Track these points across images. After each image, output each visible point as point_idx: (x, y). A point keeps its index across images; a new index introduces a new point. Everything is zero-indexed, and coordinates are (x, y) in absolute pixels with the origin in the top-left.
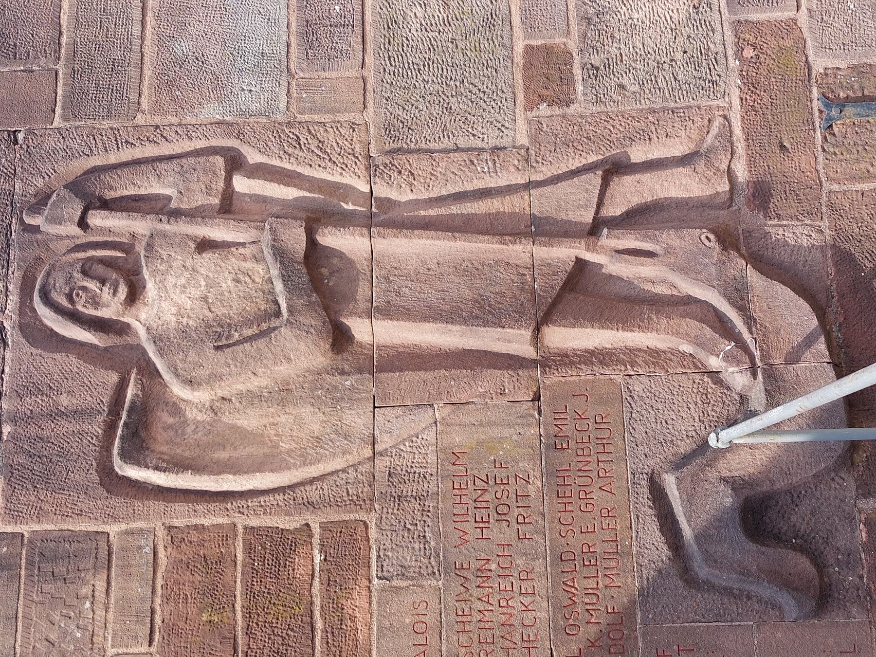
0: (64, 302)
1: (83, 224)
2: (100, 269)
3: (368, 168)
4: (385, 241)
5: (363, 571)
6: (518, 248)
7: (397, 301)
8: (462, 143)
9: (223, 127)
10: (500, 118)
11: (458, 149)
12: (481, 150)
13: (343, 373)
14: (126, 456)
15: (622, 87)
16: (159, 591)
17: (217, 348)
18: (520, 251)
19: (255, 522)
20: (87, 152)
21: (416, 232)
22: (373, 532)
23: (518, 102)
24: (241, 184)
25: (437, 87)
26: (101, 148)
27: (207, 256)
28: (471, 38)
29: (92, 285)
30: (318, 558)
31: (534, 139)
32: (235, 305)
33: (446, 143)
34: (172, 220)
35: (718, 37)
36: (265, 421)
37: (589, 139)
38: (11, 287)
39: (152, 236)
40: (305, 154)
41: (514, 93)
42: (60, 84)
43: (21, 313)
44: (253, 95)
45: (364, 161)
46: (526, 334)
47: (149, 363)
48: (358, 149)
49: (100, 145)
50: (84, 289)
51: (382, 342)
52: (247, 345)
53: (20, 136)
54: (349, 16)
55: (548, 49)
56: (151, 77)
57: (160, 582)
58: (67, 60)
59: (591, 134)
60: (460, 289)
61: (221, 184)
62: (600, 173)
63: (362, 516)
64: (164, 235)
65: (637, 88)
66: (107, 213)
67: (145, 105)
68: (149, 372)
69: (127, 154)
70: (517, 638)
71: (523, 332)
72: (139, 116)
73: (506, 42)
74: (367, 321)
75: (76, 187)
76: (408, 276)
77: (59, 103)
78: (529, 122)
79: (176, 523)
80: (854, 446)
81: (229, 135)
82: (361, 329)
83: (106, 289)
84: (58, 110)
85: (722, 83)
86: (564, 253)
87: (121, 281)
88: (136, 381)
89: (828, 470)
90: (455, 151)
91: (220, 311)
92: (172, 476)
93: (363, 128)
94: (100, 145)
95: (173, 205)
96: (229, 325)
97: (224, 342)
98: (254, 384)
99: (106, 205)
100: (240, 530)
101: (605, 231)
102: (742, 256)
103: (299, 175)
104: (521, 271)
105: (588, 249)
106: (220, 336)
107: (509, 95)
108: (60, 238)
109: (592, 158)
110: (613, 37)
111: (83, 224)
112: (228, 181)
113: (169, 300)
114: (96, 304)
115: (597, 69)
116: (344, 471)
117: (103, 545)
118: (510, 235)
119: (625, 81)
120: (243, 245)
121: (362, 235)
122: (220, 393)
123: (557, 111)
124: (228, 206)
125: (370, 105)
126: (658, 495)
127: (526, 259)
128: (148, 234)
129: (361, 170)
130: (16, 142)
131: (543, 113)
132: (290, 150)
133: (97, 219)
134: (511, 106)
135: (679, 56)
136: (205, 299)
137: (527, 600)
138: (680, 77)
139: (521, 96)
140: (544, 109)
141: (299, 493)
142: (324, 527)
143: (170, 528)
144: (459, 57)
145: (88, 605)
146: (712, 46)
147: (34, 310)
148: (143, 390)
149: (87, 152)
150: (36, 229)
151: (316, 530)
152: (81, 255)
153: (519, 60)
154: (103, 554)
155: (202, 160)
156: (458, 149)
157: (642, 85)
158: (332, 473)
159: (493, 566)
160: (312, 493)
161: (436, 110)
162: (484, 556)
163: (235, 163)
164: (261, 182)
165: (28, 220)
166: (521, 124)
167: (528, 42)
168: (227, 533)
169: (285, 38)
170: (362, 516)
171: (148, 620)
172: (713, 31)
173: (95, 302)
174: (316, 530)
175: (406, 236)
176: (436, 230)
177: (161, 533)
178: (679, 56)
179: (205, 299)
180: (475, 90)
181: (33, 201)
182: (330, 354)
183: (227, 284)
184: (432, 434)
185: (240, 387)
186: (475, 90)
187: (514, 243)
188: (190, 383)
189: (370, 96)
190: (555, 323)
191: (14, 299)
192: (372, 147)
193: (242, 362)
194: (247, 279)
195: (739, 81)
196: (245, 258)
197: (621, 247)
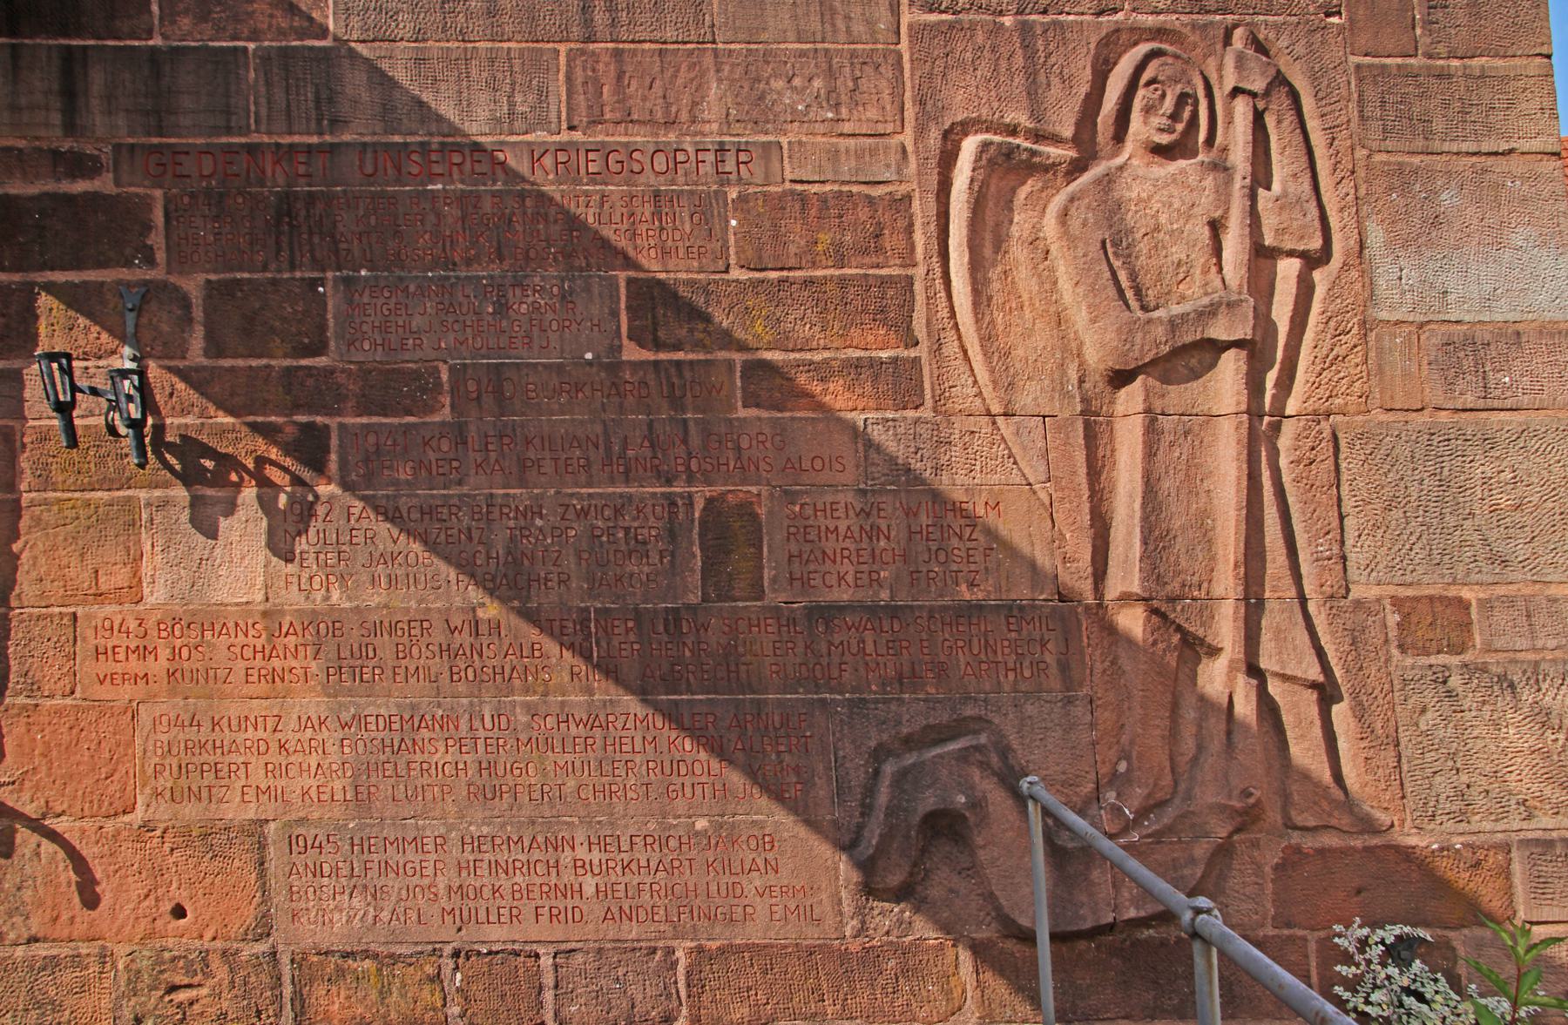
0: (1145, 77)
1: (1236, 92)
2: (1186, 114)
3: (1315, 413)
4: (1232, 431)
5: (872, 404)
6: (1231, 581)
7: (1164, 445)
8: (1349, 523)
9: (1357, 248)
10: (1381, 566)
11: (1341, 518)
12: (1342, 543)
13: (1081, 381)
14: (985, 145)
15: (1424, 711)
16: (845, 188)
17: (1103, 243)
18: (1227, 582)
19: (918, 287)
20: (1320, 95)
21: (1245, 466)
22: (910, 414)
23: (1401, 589)
24: (1288, 269)
25: (1415, 495)
26: (1326, 110)
27: (1206, 231)
28: (1476, 536)
29: (1169, 104)
30: (884, 355)
31: (1358, 603)
32: (1153, 262)
33: (1348, 506)
34: (1247, 191)
35: (1487, 826)
36: (1025, 297)
37: (1361, 669)
38: (1161, 17)
39: (1226, 169)
40: (1328, 343)
41: (1411, 584)
42: (1399, 60)
43: (1132, 29)
44: (1398, 283)
45: (1323, 409)
46: (1135, 587)
47: (1084, 169)
48: (1337, 401)
49: (1329, 109)
50: (1163, 96)
51: (1117, 426)
52: (1108, 275)
53: (1335, 20)
54: (1498, 392)
55: (1467, 626)
56: (1411, 164)
57: (855, 189)
58: (1429, 68)
59: (1366, 672)
60: (1177, 518)
61: (1288, 246)
62: (1321, 679)
63: (929, 402)
64: (1229, 182)
65: (1423, 727)
66: (1251, 118)
67: (1378, 158)
68: (1077, 168)
69: (1318, 139)
70: (812, 567)
71: (1137, 582)
72: (1365, 152)
73: (1474, 577)
74: (1140, 408)
75: (1280, 80)
76: (1193, 456)
77: (1376, 61)
78: (1378, 600)
79: (916, 204)
80: (1028, 938)
81: (1347, 254)
82: (1131, 398)
83: (1164, 121)
84: (1368, 60)
85: (1432, 826)
86: (1226, 630)
87: (1174, 137)
88: (1207, 540)
89: (998, 908)
90: (1340, 514)
91: (1143, 247)
92: (964, 197)
93: (1363, 408)
94: (1329, 109)
95: (1261, 192)
96: (1129, 256)
97: (1110, 251)
98: (1065, 285)
99: (1258, 118)
100: (910, 272)
101: (1254, 682)
102: (1230, 835)
103: (1303, 333)
104: (1205, 585)
105: (1232, 661)
106: (1116, 243)
107: (1408, 579)
108: (1220, 68)
109: (1338, 673)
110: (1484, 703)
111: (1236, 92)
112: (1291, 254)
113: (1159, 193)
114: (1148, 110)
115: (1445, 682)
116: (975, 382)
117: (890, 128)
118: (1246, 574)
119: (1429, 715)
120: (1220, 270)
121: (1238, 403)
122: (1053, 248)
123: (1393, 633)
124: (1262, 255)
125: (1390, 417)
126: (957, 729)
127: (1218, 590)
128: (1228, 164)
129: (1310, 406)
130: (1328, 15)
131: (1389, 617)
132: (1332, 324)
133: (1242, 107)
134: (1396, 580)
135: (1464, 778)
136: (1157, 229)
137: (849, 578)
138: (1438, 779)
139: (1410, 592)
140: (1393, 619)
141: (951, 335)
142: (916, 360)
143: (908, 198)
144: (1451, 521)
145: (830, 115)
146: (1477, 817)
147: (1136, 44)
148: (1054, 164)
149: (1320, 95)
150: (1227, 41)
151: (913, 353)
152: (1201, 93)
153: (1452, 592)
154: (880, 128)
155: (1317, 224)
156: (1341, 518)
157: (1425, 734)
158: (972, 370)
159: (882, 543)
160: (951, 348)
161: (1387, 492)
162: (893, 534)
163: (1312, 261)
164: (1294, 291)
165: (1238, 33)
166: (1375, 591)
167: (1474, 603)
168: (908, 259)
169: (1467, 318)
170: (929, 402)
171: (816, 178)
172: (1496, 820)
173: (1148, 110)
174: (913, 353)
175: (1239, 454)
176: (1249, 489)
177: (903, 189)
178: (1464, 778)
179: (1157, 229)
180: (1413, 539)
181: (1261, 37)
182: (1102, 367)
183: (1178, 252)
184: (1018, 480)
185: (1062, 269)
186: (1413, 539)
187: (1236, 576)
188: (1064, 214)
189: (1400, 416)
190: (1148, 620)
191: (1150, 20)
192: (1339, 418)
193: (1089, 270)
194: (1181, 276)
195: (1435, 846)
196: (1206, 272)
197: (1236, 699)
